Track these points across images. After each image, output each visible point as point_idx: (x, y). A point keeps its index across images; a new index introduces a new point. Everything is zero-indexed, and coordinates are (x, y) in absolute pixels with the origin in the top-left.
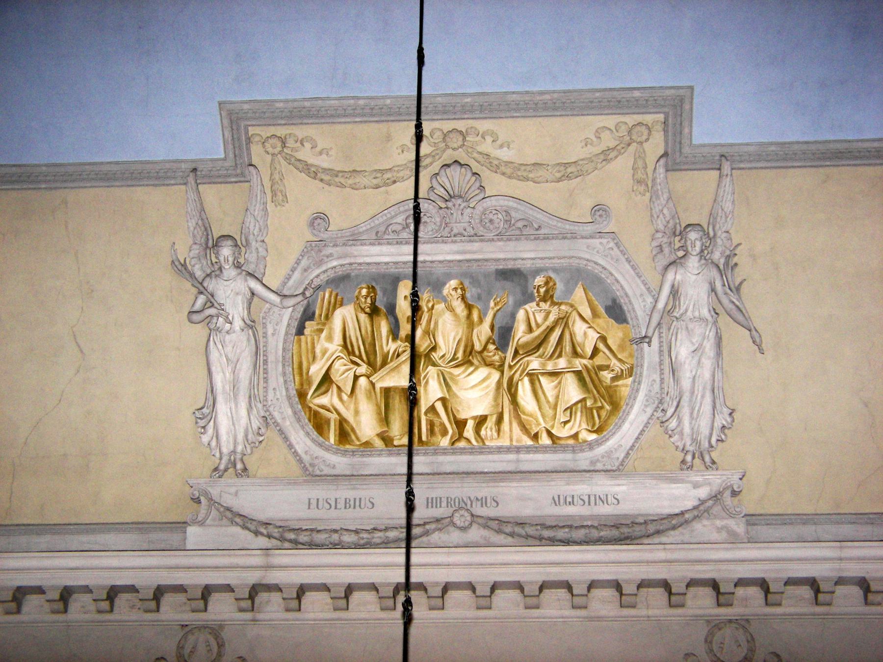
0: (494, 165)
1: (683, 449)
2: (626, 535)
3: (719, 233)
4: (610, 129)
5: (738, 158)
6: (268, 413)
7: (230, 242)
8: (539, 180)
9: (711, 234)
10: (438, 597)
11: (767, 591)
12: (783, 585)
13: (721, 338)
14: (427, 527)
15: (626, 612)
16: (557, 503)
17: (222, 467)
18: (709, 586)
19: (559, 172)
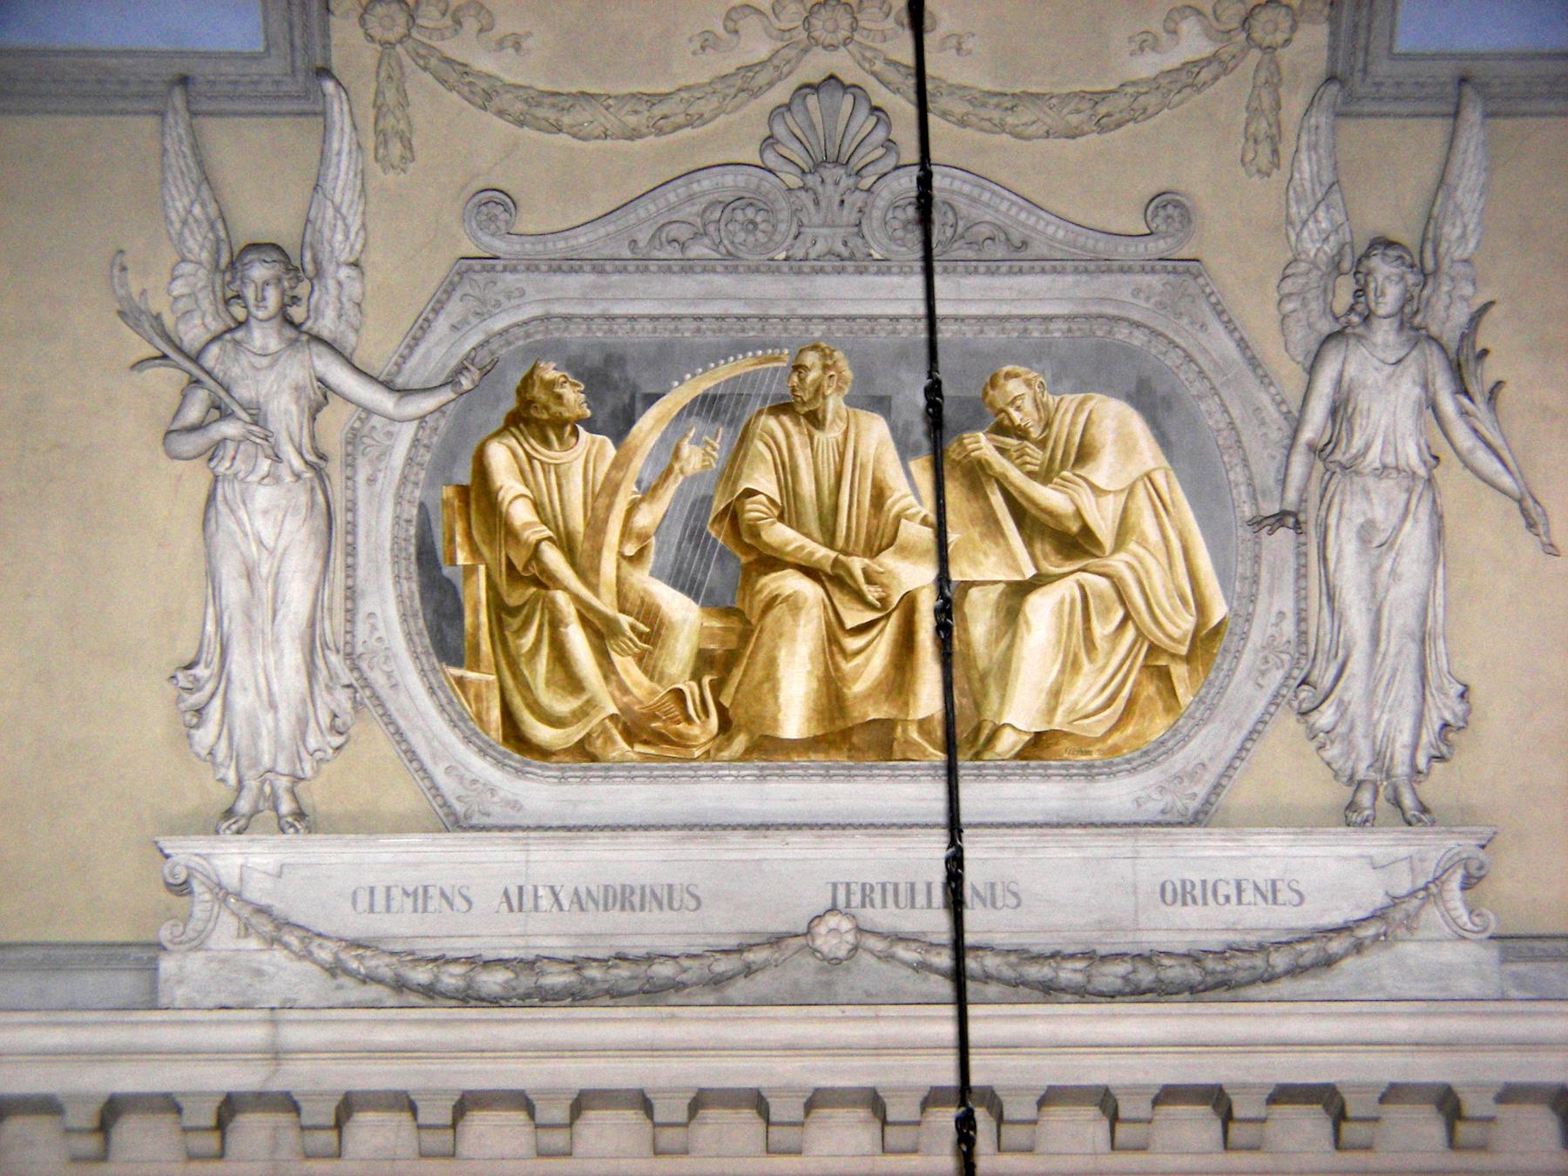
0: (478, 89)
1: (1351, 778)
2: (1219, 977)
3: (330, 268)
4: (1199, 12)
8: (1031, 130)
9: (1430, 264)
10: (330, 1128)
11: (1339, 1116)
13: (1441, 517)
14: (750, 956)
15: (665, 1164)
16: (515, 903)
17: (244, 806)
18: (1430, 1103)
19: (1078, 111)
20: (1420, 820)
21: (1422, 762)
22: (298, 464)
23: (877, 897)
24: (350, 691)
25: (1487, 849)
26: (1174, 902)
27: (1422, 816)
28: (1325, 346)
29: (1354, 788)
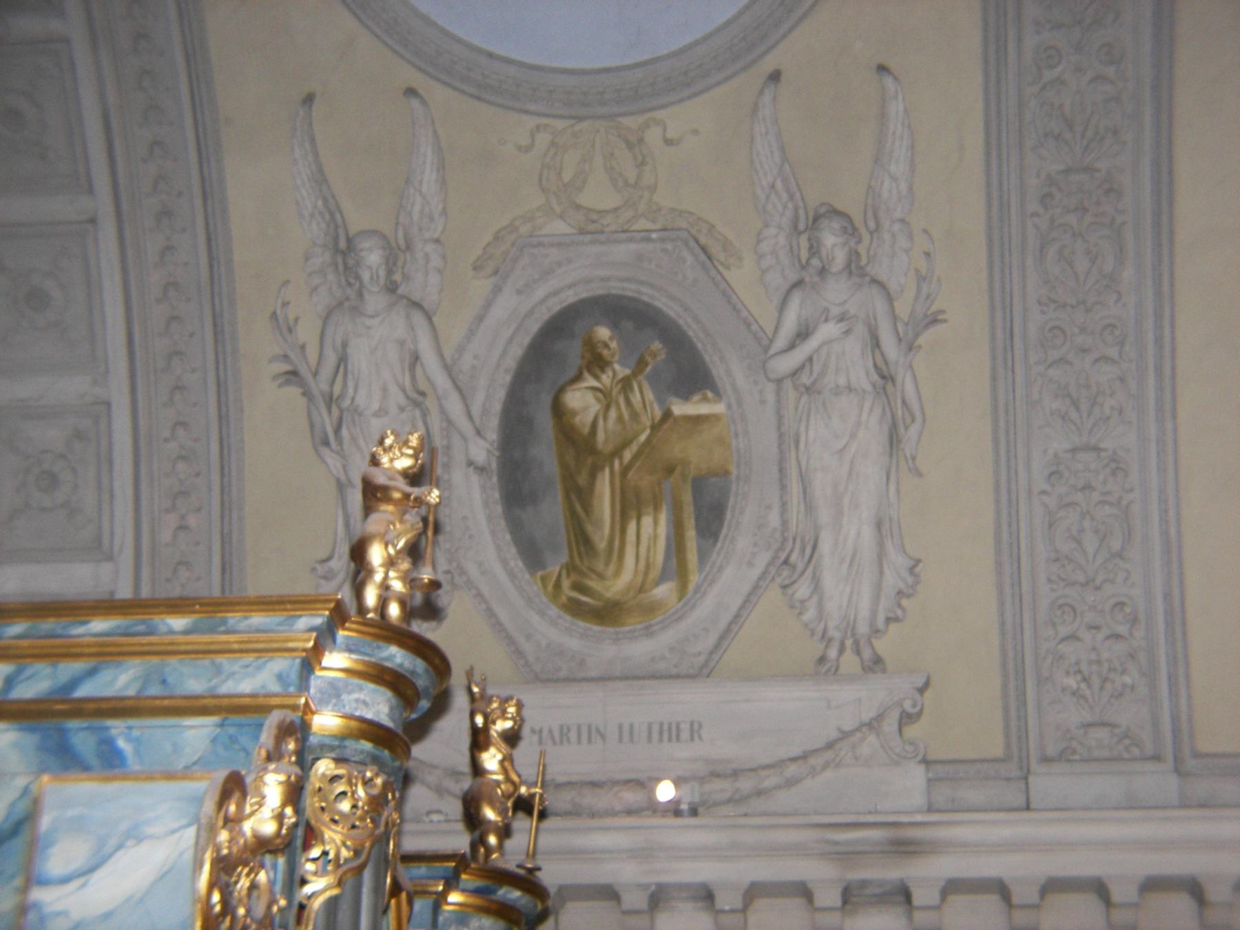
6: (455, 564)
7: (836, 224)
23: (573, 735)
26: (561, 742)
27: (876, 664)
29: (824, 644)
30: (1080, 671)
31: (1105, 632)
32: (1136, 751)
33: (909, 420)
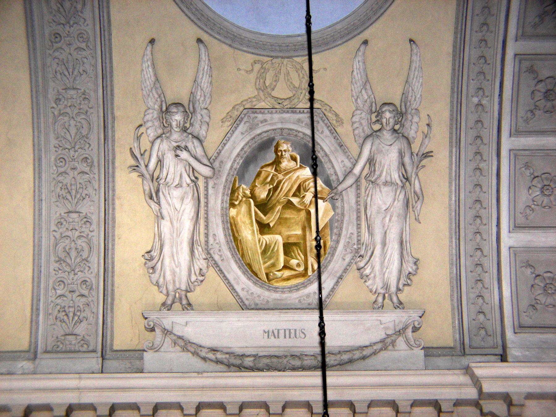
3: (198, 110)
5: (277, 48)
12: (452, 405)
17: (169, 302)
20: (398, 307)
21: (401, 286)
22: (188, 181)
24: (207, 261)
25: (422, 318)
28: (366, 140)
30: (65, 311)
31: (77, 293)
32: (85, 348)
33: (416, 198)
